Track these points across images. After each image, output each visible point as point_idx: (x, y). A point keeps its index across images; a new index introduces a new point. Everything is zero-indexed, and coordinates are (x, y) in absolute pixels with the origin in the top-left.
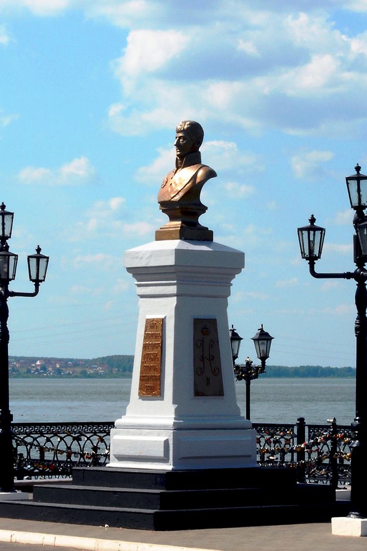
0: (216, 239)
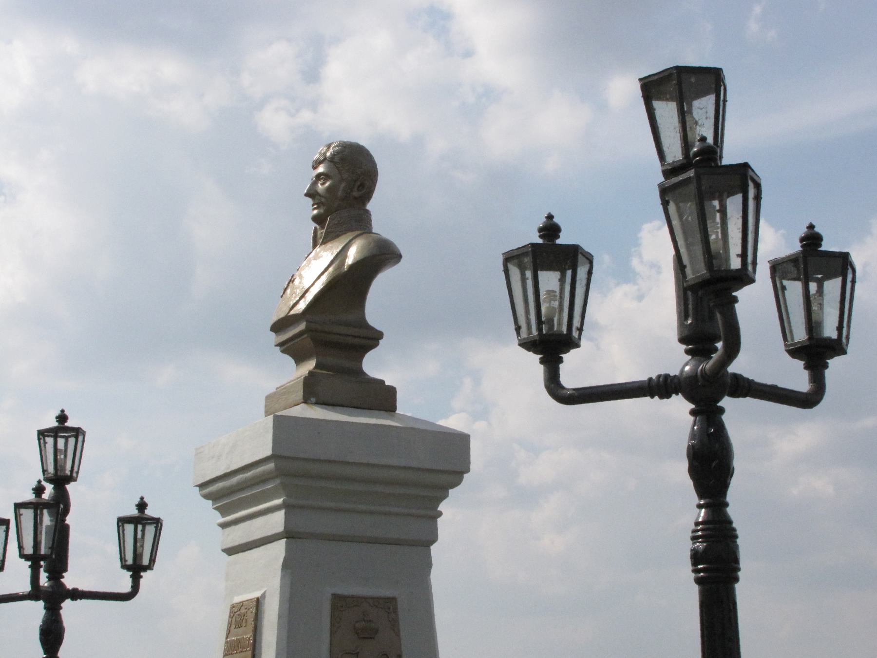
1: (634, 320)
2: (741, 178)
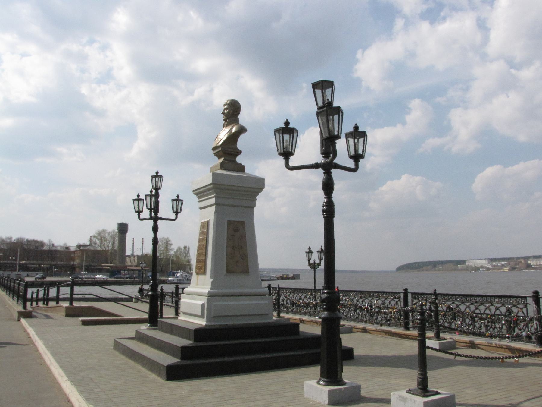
0: (247, 171)
1: (309, 147)
2: (338, 110)
